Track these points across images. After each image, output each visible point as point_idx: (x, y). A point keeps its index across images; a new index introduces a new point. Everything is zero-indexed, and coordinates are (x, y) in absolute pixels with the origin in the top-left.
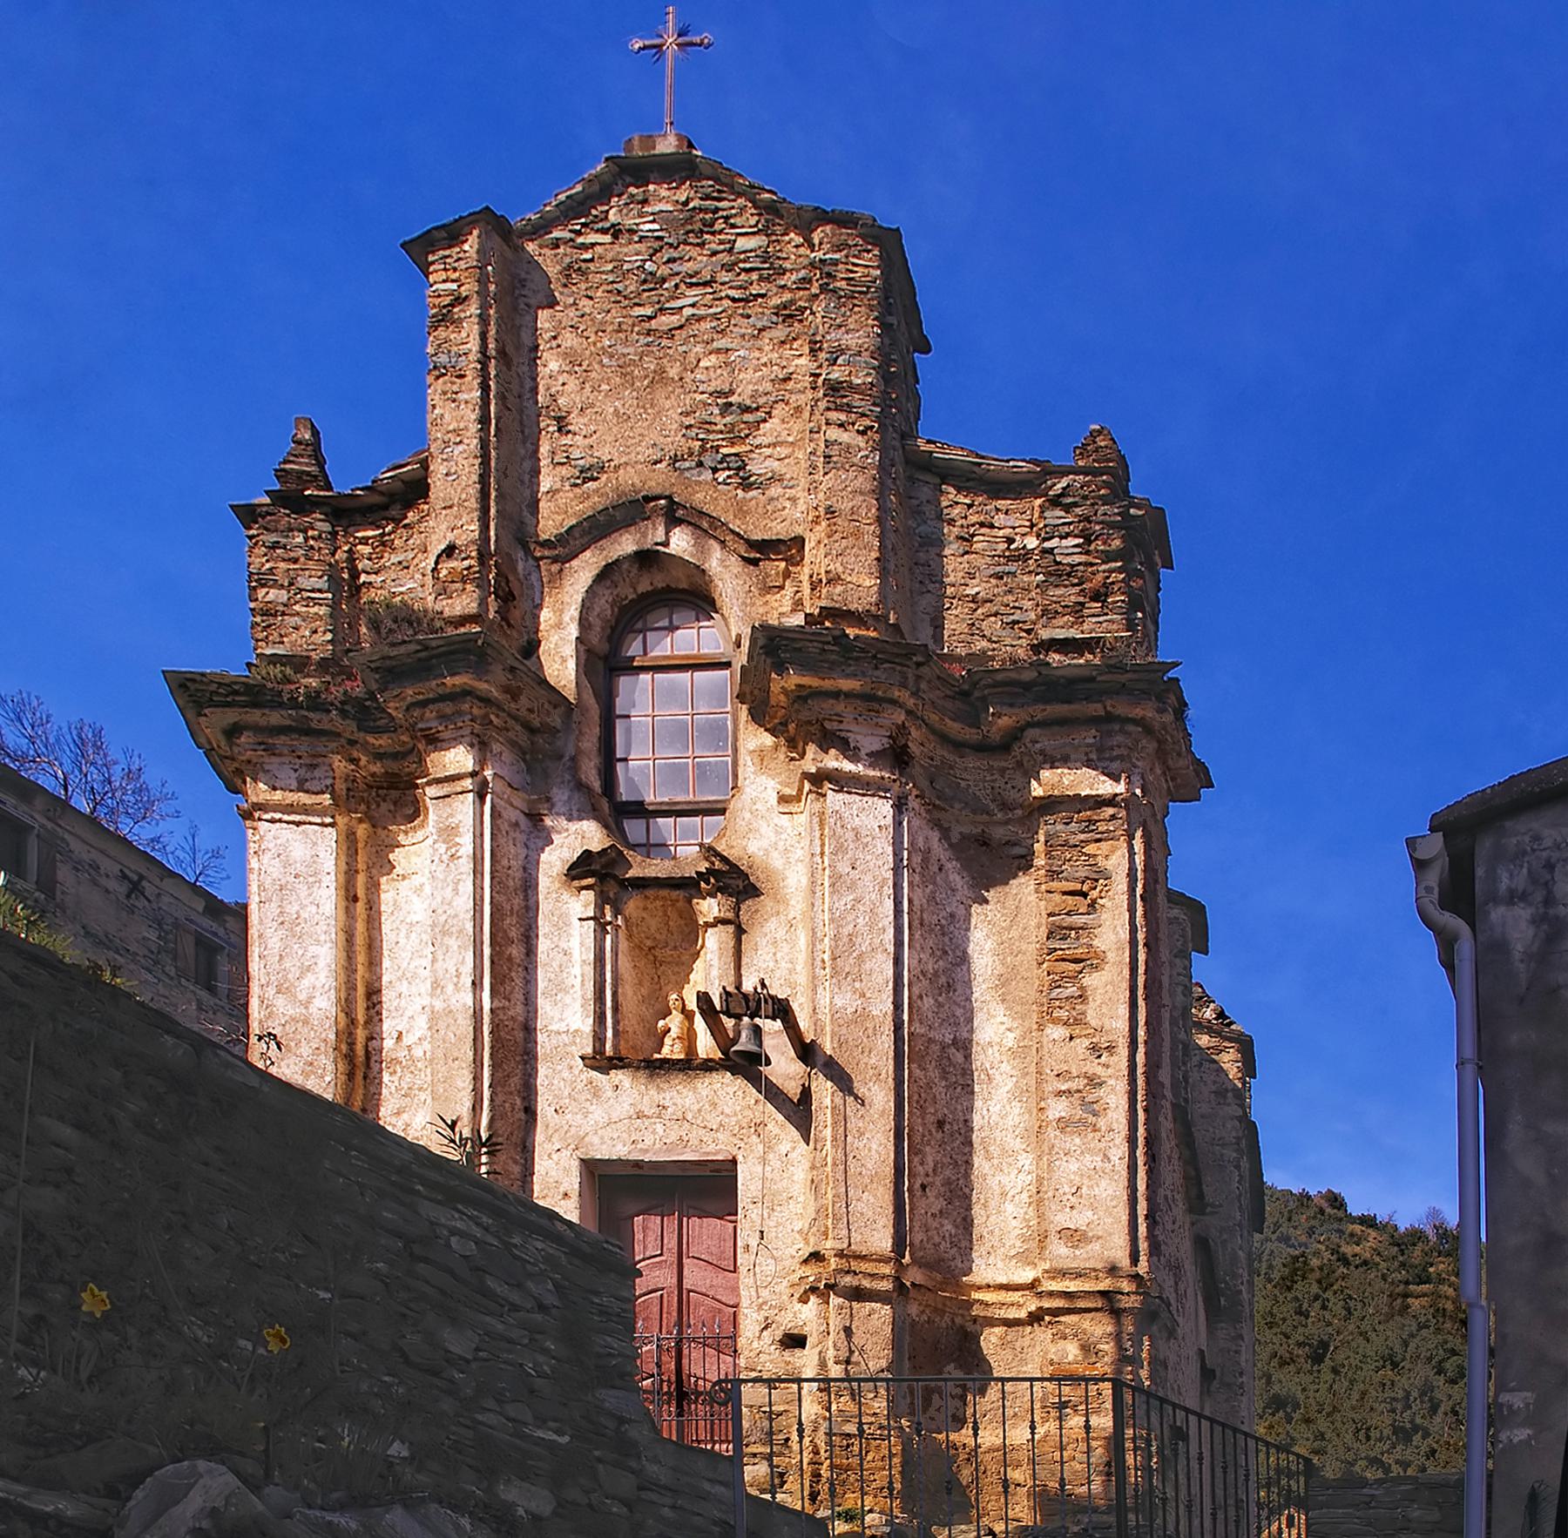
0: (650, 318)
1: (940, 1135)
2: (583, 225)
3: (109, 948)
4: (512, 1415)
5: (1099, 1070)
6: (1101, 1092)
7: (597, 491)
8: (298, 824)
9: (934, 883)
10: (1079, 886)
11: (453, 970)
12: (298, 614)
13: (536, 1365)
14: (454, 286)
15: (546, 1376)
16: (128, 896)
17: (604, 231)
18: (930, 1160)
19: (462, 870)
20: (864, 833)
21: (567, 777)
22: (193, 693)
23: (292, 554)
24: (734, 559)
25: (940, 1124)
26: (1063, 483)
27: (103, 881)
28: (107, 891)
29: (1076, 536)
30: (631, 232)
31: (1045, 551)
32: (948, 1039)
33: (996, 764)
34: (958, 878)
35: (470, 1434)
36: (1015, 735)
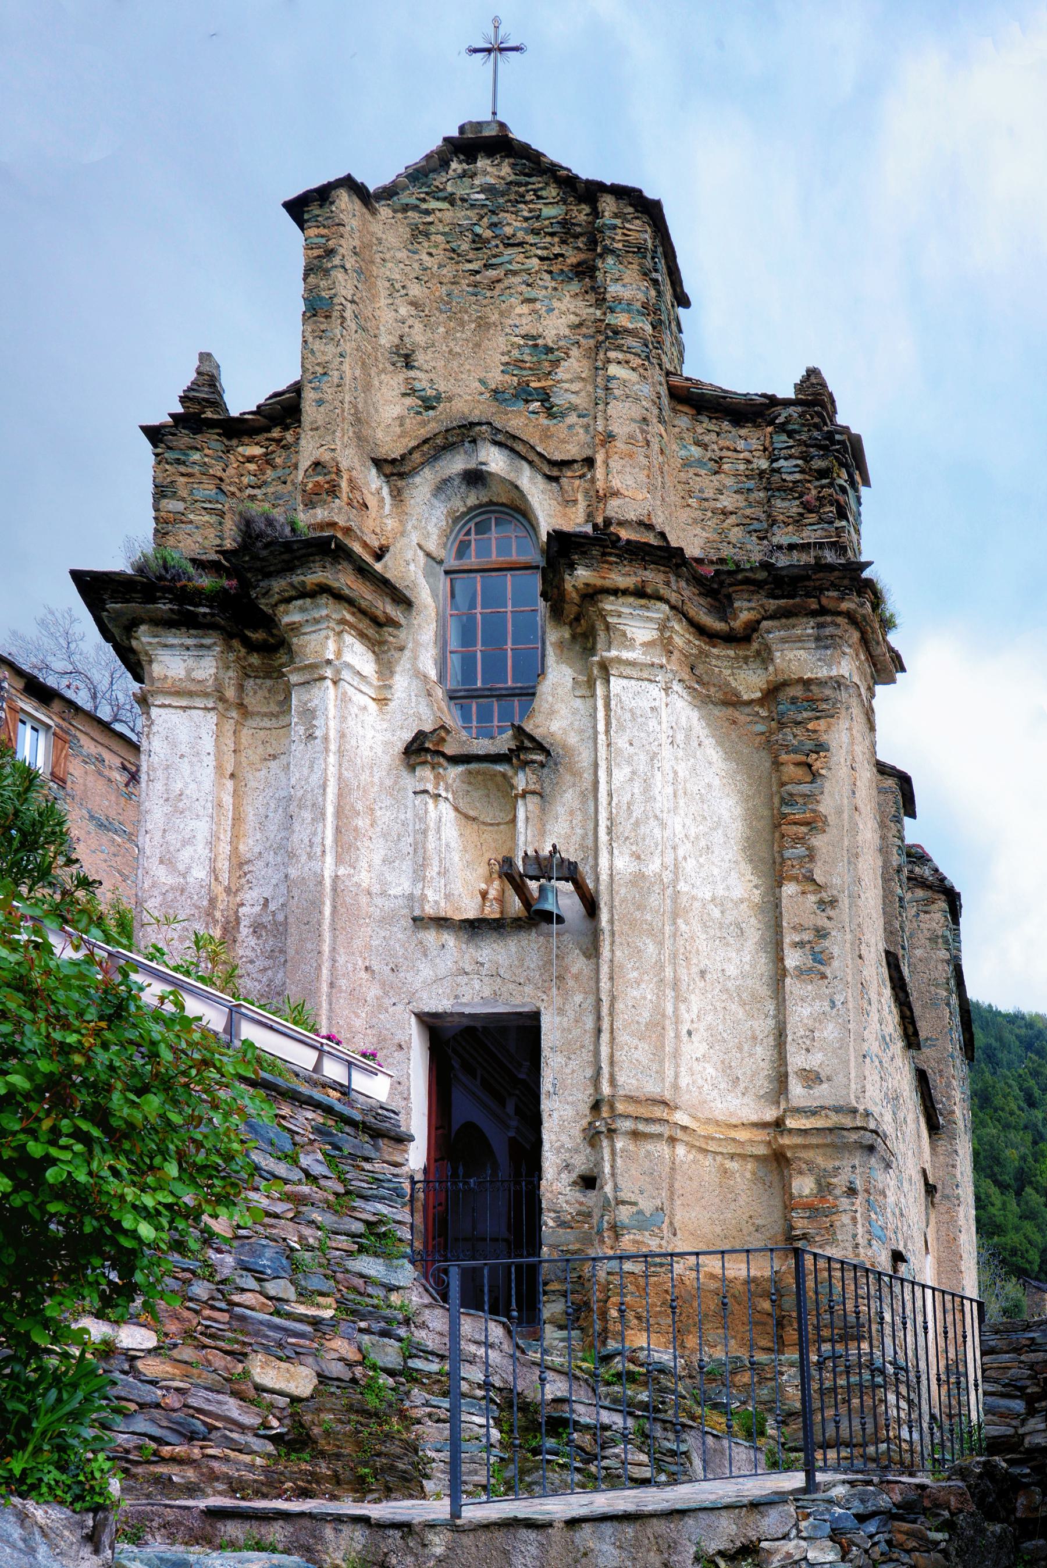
0: (477, 272)
1: (702, 984)
2: (427, 193)
3: (109, 830)
4: (272, 1293)
5: (827, 924)
6: (826, 943)
7: (434, 419)
8: (184, 708)
9: (695, 757)
10: (803, 758)
11: (306, 841)
12: (191, 522)
13: (302, 1238)
14: (323, 240)
15: (310, 1248)
16: (127, 785)
17: (444, 199)
18: (695, 1009)
19: (317, 749)
20: (639, 713)
21: (408, 666)
22: (93, 587)
23: (190, 470)
24: (539, 478)
25: (703, 973)
26: (784, 414)
27: (106, 772)
28: (110, 780)
29: (797, 458)
30: (463, 200)
31: (774, 470)
32: (708, 896)
33: (741, 653)
34: (713, 753)
35: (225, 1317)
36: (753, 627)
